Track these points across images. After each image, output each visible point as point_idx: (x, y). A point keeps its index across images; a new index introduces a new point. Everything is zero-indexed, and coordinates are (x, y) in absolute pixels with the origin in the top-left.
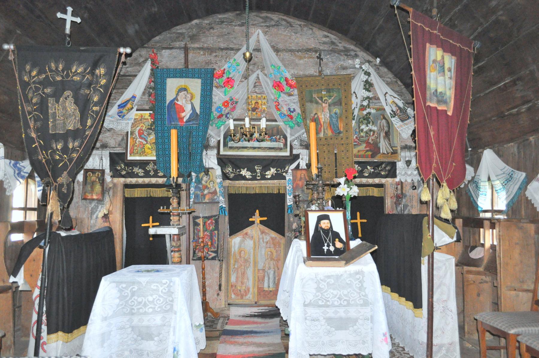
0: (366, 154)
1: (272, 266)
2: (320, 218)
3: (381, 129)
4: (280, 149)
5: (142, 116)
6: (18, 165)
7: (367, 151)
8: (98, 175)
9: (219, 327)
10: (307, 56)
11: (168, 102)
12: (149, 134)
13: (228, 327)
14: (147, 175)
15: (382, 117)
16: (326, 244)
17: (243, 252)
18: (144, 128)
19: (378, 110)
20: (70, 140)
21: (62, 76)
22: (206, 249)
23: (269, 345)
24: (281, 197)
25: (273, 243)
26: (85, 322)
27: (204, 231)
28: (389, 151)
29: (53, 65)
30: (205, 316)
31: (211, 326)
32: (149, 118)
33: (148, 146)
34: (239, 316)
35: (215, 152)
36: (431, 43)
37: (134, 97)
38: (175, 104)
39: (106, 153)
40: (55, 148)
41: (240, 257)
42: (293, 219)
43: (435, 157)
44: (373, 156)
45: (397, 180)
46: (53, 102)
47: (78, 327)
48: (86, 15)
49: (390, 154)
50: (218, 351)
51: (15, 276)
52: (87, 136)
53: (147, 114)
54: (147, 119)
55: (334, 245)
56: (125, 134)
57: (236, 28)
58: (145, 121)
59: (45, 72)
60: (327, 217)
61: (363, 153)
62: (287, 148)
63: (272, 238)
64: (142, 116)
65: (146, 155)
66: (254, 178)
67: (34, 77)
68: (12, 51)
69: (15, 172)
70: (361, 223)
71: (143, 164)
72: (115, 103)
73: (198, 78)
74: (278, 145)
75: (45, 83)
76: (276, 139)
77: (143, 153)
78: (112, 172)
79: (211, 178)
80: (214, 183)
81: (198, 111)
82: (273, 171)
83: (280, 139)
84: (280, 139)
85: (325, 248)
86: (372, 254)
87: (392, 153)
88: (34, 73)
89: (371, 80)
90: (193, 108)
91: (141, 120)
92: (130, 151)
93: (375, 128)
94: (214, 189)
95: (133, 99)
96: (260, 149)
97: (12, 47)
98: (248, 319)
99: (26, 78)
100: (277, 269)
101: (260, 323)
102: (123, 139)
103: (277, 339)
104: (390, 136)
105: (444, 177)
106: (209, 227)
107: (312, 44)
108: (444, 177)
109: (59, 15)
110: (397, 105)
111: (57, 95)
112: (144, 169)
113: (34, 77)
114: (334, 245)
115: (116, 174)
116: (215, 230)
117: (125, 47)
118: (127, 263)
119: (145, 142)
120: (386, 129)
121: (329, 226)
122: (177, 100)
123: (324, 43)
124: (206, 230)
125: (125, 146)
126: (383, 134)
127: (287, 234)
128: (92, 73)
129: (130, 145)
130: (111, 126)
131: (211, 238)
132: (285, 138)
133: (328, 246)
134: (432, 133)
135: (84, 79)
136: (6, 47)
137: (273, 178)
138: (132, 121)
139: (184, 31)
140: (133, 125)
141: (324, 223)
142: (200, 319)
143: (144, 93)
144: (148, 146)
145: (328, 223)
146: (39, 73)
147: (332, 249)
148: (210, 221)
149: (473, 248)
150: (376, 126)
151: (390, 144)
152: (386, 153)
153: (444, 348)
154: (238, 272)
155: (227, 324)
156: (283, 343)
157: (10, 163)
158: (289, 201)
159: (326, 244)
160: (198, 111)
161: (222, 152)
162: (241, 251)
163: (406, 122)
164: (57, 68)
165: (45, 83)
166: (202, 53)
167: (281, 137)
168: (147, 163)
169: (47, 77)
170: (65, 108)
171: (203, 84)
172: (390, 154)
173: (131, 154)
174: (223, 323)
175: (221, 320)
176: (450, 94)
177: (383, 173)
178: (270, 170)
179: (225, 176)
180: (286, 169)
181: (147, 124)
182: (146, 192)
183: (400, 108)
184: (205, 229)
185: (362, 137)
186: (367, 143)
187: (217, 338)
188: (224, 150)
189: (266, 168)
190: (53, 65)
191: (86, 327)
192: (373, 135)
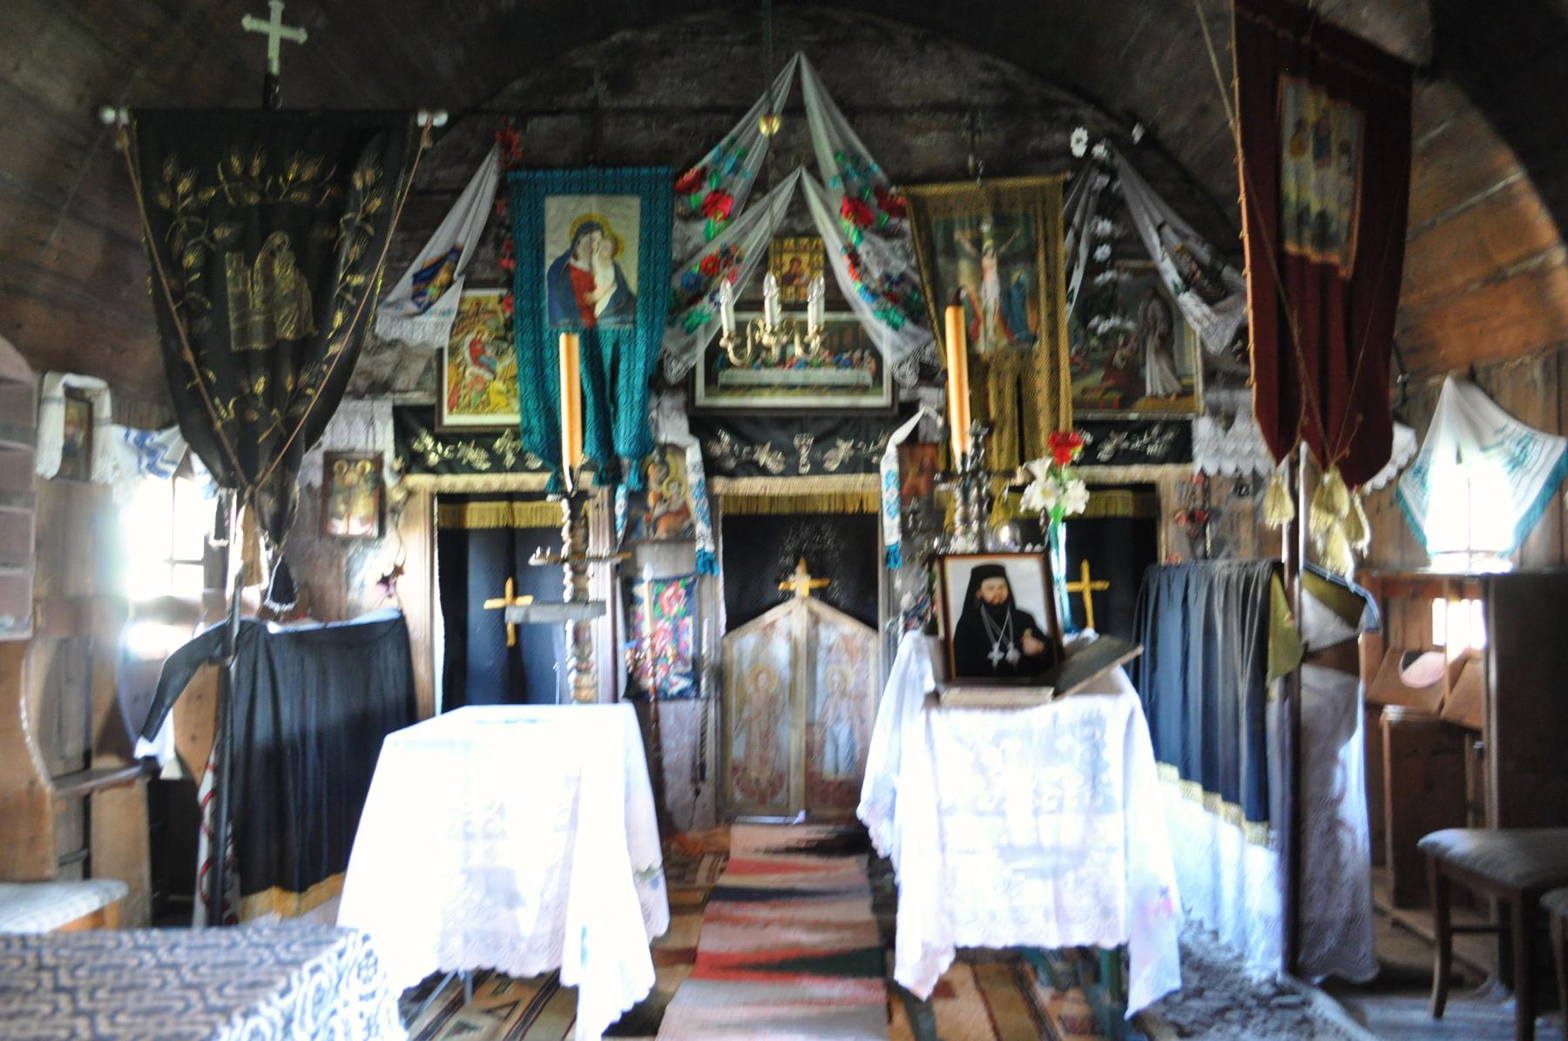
0: (1106, 397)
1: (844, 714)
2: (979, 575)
3: (1146, 328)
4: (863, 389)
5: (478, 304)
6: (148, 442)
7: (1108, 390)
8: (364, 468)
9: (701, 878)
10: (935, 124)
11: (549, 262)
12: (500, 354)
13: (726, 880)
14: (497, 465)
15: (1149, 292)
16: (996, 646)
17: (763, 677)
18: (485, 337)
19: (1137, 273)
20: (287, 366)
21: (262, 194)
22: (661, 666)
23: (840, 926)
24: (867, 523)
25: (847, 650)
26: (337, 860)
27: (655, 620)
28: (1170, 389)
29: (236, 163)
30: (665, 850)
31: (680, 878)
32: (499, 308)
33: (498, 385)
34: (757, 851)
35: (680, 399)
36: (1296, 73)
37: (456, 251)
38: (570, 268)
39: (383, 409)
40: (248, 391)
41: (757, 688)
42: (903, 584)
43: (1304, 397)
44: (1126, 402)
45: (1196, 468)
46: (238, 264)
47: (317, 879)
48: (320, 22)
49: (1173, 397)
50: (701, 943)
51: (151, 740)
52: (333, 357)
53: (491, 295)
54: (493, 312)
55: (1019, 646)
56: (434, 353)
57: (735, 50)
58: (486, 316)
59: (216, 183)
60: (999, 571)
61: (1096, 396)
62: (881, 384)
63: (844, 638)
64: (478, 304)
65: (492, 412)
66: (791, 470)
67: (184, 197)
68: (124, 126)
69: (140, 462)
70: (1094, 593)
71: (484, 437)
72: (406, 269)
73: (632, 192)
74: (858, 377)
75: (208, 213)
76: (851, 358)
77: (484, 405)
78: (400, 459)
79: (673, 471)
80: (680, 485)
81: (633, 284)
82: (844, 448)
83: (862, 359)
84: (862, 359)
85: (995, 655)
86: (1126, 667)
87: (1179, 396)
88: (184, 186)
89: (1119, 189)
90: (620, 279)
91: (477, 314)
92: (449, 400)
93: (1130, 325)
94: (680, 502)
95: (453, 257)
96: (807, 390)
97: (124, 117)
98: (779, 859)
99: (164, 200)
100: (857, 722)
101: (815, 869)
102: (428, 369)
103: (860, 911)
104: (1175, 347)
105: (1332, 451)
106: (671, 606)
107: (948, 90)
108: (1332, 451)
109: (249, 23)
110: (1194, 258)
111: (246, 247)
112: (489, 449)
113: (184, 197)
114: (1019, 646)
115: (414, 462)
116: (687, 613)
117: (433, 109)
118: (448, 706)
119: (487, 376)
120: (1161, 328)
121: (1005, 593)
122: (576, 258)
123: (984, 85)
124: (662, 616)
125: (434, 387)
126: (1152, 343)
127: (884, 624)
128: (344, 181)
129: (449, 384)
130: (395, 333)
131: (676, 632)
132: (877, 357)
133: (1004, 649)
134: (1296, 333)
135: (321, 198)
136: (109, 115)
137: (848, 467)
138: (453, 317)
139: (591, 62)
140: (456, 329)
141: (991, 588)
142: (652, 854)
143: (483, 241)
144: (498, 385)
145: (1000, 588)
146: (196, 189)
147: (1012, 655)
148: (670, 592)
149: (1412, 657)
150: (1134, 318)
151: (1173, 370)
152: (1161, 392)
153: (1330, 933)
154: (750, 728)
155: (722, 871)
156: (879, 922)
157: (127, 436)
158: (891, 533)
159: (996, 646)
160: (633, 284)
161: (701, 398)
162: (760, 672)
163: (1221, 304)
164: (247, 168)
165: (208, 213)
166: (641, 123)
167: (867, 353)
168: (494, 432)
169: (220, 194)
170: (268, 279)
171: (646, 213)
172: (1173, 397)
173: (451, 410)
174: (711, 869)
175: (707, 861)
176: (1343, 217)
177: (1151, 450)
178: (836, 447)
179: (712, 467)
180: (881, 443)
181: (492, 324)
182: (494, 514)
183: (1201, 266)
184: (657, 613)
185: (1095, 350)
186: (1108, 365)
187: (698, 908)
188: (708, 394)
189: (824, 440)
190: (236, 163)
191: (344, 877)
192: (1125, 344)
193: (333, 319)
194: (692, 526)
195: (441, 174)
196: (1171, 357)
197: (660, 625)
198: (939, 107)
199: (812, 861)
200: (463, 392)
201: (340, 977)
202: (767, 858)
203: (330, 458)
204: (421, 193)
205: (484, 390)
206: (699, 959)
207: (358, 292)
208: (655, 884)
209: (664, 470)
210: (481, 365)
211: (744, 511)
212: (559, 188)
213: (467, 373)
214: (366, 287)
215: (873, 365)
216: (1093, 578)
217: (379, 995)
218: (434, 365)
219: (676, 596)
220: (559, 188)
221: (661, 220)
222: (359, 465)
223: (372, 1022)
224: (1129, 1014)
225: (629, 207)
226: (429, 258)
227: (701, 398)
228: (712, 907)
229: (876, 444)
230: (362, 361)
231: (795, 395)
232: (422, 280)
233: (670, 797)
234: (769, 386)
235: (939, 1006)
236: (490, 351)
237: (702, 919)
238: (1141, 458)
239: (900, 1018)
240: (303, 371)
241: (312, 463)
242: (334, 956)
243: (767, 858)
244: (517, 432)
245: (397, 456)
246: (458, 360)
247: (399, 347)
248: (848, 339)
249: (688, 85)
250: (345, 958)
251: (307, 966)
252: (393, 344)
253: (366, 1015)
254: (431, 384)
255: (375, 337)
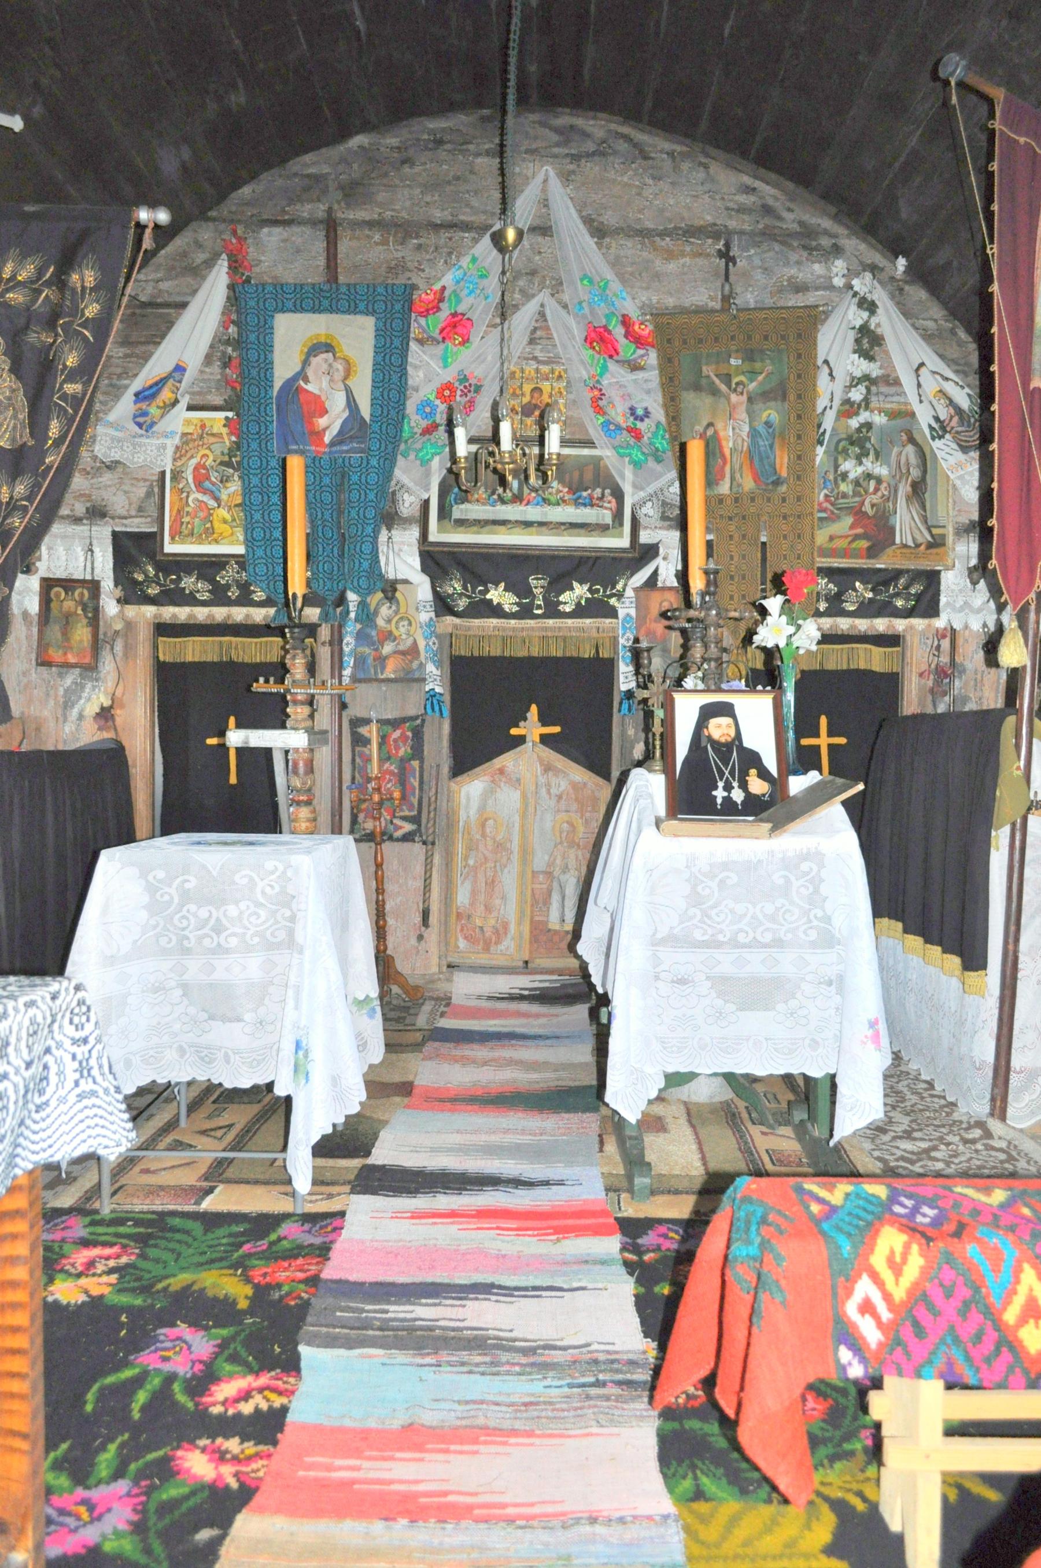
0: (854, 545)
2: (708, 712)
3: (900, 471)
4: (603, 529)
5: (203, 427)
7: (856, 537)
9: (421, 1021)
10: (688, 249)
11: (278, 384)
12: (225, 480)
14: (219, 597)
17: (491, 822)
18: (209, 462)
19: (893, 415)
27: (382, 761)
32: (225, 431)
33: (223, 513)
34: (479, 997)
37: (180, 369)
38: (299, 390)
39: (102, 534)
44: (872, 552)
49: (923, 547)
54: (219, 435)
55: (744, 786)
56: (155, 478)
57: (479, 160)
58: (212, 440)
60: (726, 710)
61: (842, 544)
62: (621, 524)
63: (574, 785)
66: (525, 612)
72: (127, 387)
73: (367, 313)
77: (209, 534)
79: (402, 610)
81: (366, 412)
82: (580, 591)
83: (602, 498)
84: (602, 498)
85: (719, 794)
87: (930, 546)
89: (878, 325)
90: (352, 403)
91: (201, 437)
92: (171, 528)
95: (177, 375)
96: (544, 529)
101: (537, 1016)
102: (149, 494)
106: (397, 748)
107: (705, 211)
114: (744, 786)
116: (413, 757)
119: (212, 503)
120: (915, 473)
122: (306, 380)
123: (742, 210)
124: (389, 758)
128: (60, 282)
130: (115, 455)
132: (619, 495)
133: (728, 788)
137: (580, 611)
138: (177, 441)
139: (326, 169)
140: (179, 453)
141: (719, 726)
143: (208, 359)
144: (223, 513)
145: (728, 726)
148: (397, 734)
152: (911, 543)
154: (475, 876)
155: (442, 1015)
159: (721, 784)
160: (366, 412)
162: (486, 820)
166: (377, 237)
167: (607, 491)
168: (217, 563)
171: (380, 333)
172: (923, 547)
173: (173, 538)
175: (427, 1007)
178: (572, 589)
179: (443, 605)
180: (619, 587)
181: (217, 449)
182: (217, 649)
185: (844, 496)
186: (858, 513)
188: (440, 530)
189: (560, 582)
192: (877, 490)
193: (47, 428)
194: (422, 666)
195: (164, 286)
196: (924, 507)
197: (386, 766)
198: (692, 232)
199: (535, 1008)
200: (186, 519)
201: (54, 1017)
202: (484, 1004)
203: (48, 584)
204: (144, 305)
205: (208, 518)
206: (415, 1091)
207: (76, 401)
208: (371, 1014)
209: (394, 608)
210: (205, 492)
211: (476, 654)
212: (289, 304)
213: (190, 500)
214: (84, 394)
215: (614, 505)
216: (831, 734)
217: (92, 1040)
218: (156, 490)
219: (404, 738)
220: (289, 304)
221: (397, 342)
222: (77, 593)
223: (84, 1064)
224: (832, 1143)
225: (363, 328)
226: (154, 374)
227: (435, 535)
228: (430, 1047)
229: (614, 587)
230: (78, 482)
231: (531, 534)
232: (146, 398)
233: (391, 941)
234: (503, 523)
235: (649, 1139)
236: (214, 477)
237: (421, 1056)
238: (885, 609)
239: (611, 1147)
240: (17, 482)
241: (28, 590)
242: (48, 997)
243: (484, 1004)
244: (241, 561)
245: (116, 586)
246: (181, 486)
247: (120, 469)
248: (589, 476)
249: (428, 198)
250: (58, 1002)
251: (22, 1001)
252: (112, 466)
253: (79, 1057)
254: (153, 511)
255: (95, 458)
